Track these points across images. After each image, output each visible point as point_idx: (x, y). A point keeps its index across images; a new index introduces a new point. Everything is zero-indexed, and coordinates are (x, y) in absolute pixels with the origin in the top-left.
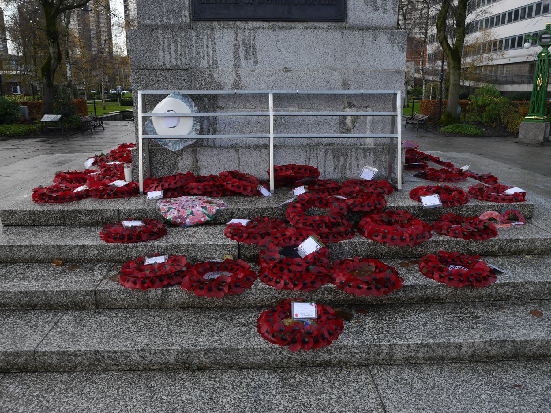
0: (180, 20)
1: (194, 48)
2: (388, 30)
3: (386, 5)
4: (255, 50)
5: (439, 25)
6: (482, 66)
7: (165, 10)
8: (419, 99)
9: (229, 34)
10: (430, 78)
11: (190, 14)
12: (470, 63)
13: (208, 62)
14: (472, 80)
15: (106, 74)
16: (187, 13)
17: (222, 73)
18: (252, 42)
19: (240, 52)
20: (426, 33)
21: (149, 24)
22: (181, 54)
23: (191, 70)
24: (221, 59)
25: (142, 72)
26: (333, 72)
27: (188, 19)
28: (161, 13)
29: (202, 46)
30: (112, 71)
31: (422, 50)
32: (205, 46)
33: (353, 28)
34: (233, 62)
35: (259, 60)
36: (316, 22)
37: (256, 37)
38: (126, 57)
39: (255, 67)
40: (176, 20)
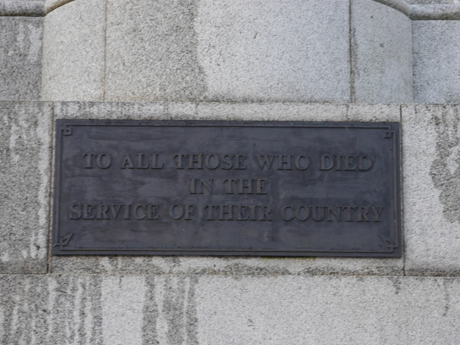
0: (25, 253)
1: (49, 318)
4: (193, 322)
11: (48, 241)
16: (42, 240)
18: (186, 304)
19: (158, 327)
29: (71, 312)
32: (76, 313)
33: (421, 273)
36: (335, 257)
37: (197, 291)
40: (16, 252)
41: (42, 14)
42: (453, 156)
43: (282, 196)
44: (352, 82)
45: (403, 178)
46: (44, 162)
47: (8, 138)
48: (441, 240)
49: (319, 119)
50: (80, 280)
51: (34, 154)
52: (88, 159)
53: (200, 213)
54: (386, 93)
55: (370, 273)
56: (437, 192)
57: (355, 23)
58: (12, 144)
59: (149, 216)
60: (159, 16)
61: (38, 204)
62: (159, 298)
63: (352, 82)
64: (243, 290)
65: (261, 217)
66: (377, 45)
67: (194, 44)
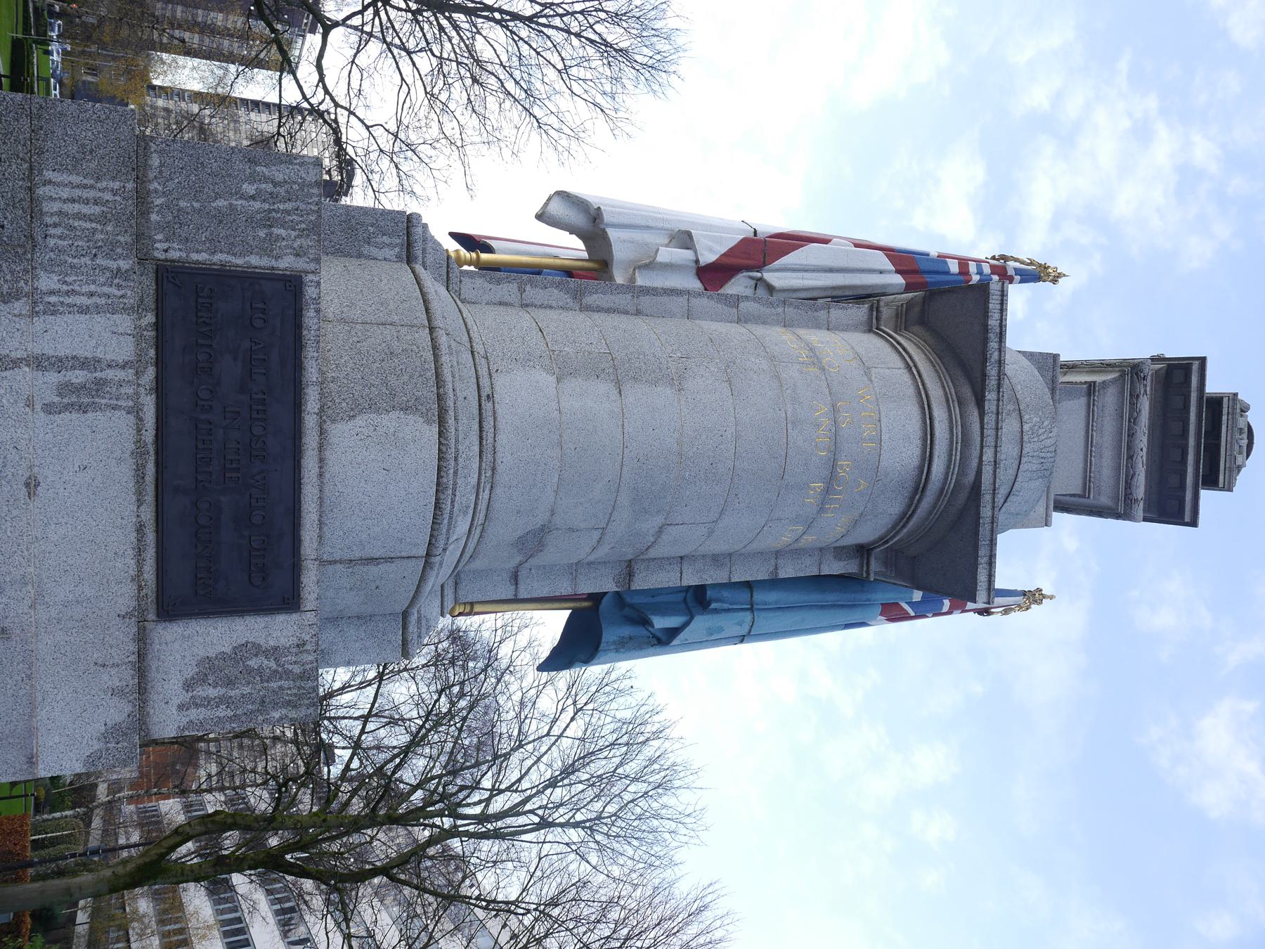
0: (159, 237)
1: (87, 260)
2: (141, 719)
3: (197, 706)
4: (83, 409)
5: (217, 818)
6: (128, 941)
7: (182, 204)
8: (38, 809)
9: (124, 349)
10: (97, 823)
11: (174, 261)
12: (135, 911)
13: (52, 293)
14: (92, 930)
15: (102, 20)
16: (174, 255)
17: (22, 324)
18: (103, 401)
19: (77, 372)
20: (210, 791)
21: (150, 162)
22: (72, 228)
23: (29, 246)
24: (59, 324)
25: (25, 122)
26: (28, 602)
27: (161, 256)
28: (175, 195)
29: (94, 282)
30: (107, 39)
31: (164, 790)
32: (93, 288)
33: (142, 639)
34: (51, 353)
35: (58, 418)
36: (157, 552)
37: (118, 413)
38: (148, 80)
39: (38, 407)
40: (160, 227)
41: (409, 262)
42: (266, 662)
43: (222, 498)
44: (341, 562)
45: (243, 616)
46: (257, 261)
47: (283, 226)
48: (178, 656)
49: (302, 533)
50: (129, 293)
51: (265, 251)
52: (260, 305)
53: (203, 417)
54: (330, 594)
55: (140, 588)
56: (228, 649)
57: (398, 562)
58: (276, 231)
59: (200, 365)
60: (406, 378)
61: (213, 253)
62: (110, 374)
63: (341, 562)
64: (120, 460)
65: (199, 478)
66: (378, 583)
67: (378, 411)
